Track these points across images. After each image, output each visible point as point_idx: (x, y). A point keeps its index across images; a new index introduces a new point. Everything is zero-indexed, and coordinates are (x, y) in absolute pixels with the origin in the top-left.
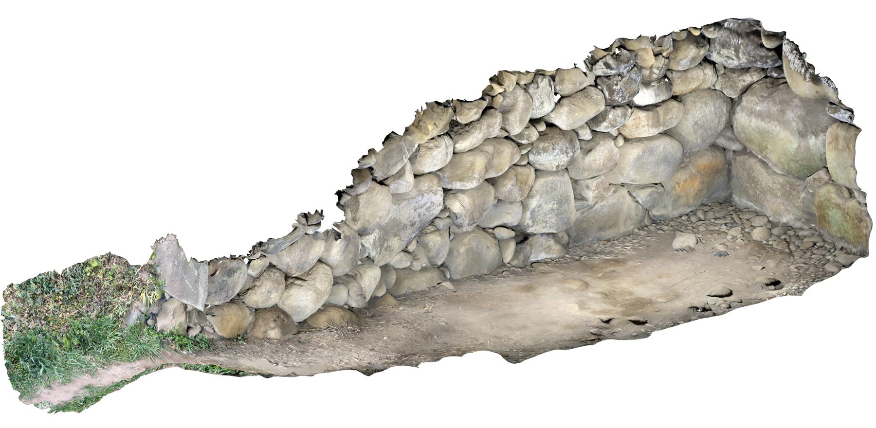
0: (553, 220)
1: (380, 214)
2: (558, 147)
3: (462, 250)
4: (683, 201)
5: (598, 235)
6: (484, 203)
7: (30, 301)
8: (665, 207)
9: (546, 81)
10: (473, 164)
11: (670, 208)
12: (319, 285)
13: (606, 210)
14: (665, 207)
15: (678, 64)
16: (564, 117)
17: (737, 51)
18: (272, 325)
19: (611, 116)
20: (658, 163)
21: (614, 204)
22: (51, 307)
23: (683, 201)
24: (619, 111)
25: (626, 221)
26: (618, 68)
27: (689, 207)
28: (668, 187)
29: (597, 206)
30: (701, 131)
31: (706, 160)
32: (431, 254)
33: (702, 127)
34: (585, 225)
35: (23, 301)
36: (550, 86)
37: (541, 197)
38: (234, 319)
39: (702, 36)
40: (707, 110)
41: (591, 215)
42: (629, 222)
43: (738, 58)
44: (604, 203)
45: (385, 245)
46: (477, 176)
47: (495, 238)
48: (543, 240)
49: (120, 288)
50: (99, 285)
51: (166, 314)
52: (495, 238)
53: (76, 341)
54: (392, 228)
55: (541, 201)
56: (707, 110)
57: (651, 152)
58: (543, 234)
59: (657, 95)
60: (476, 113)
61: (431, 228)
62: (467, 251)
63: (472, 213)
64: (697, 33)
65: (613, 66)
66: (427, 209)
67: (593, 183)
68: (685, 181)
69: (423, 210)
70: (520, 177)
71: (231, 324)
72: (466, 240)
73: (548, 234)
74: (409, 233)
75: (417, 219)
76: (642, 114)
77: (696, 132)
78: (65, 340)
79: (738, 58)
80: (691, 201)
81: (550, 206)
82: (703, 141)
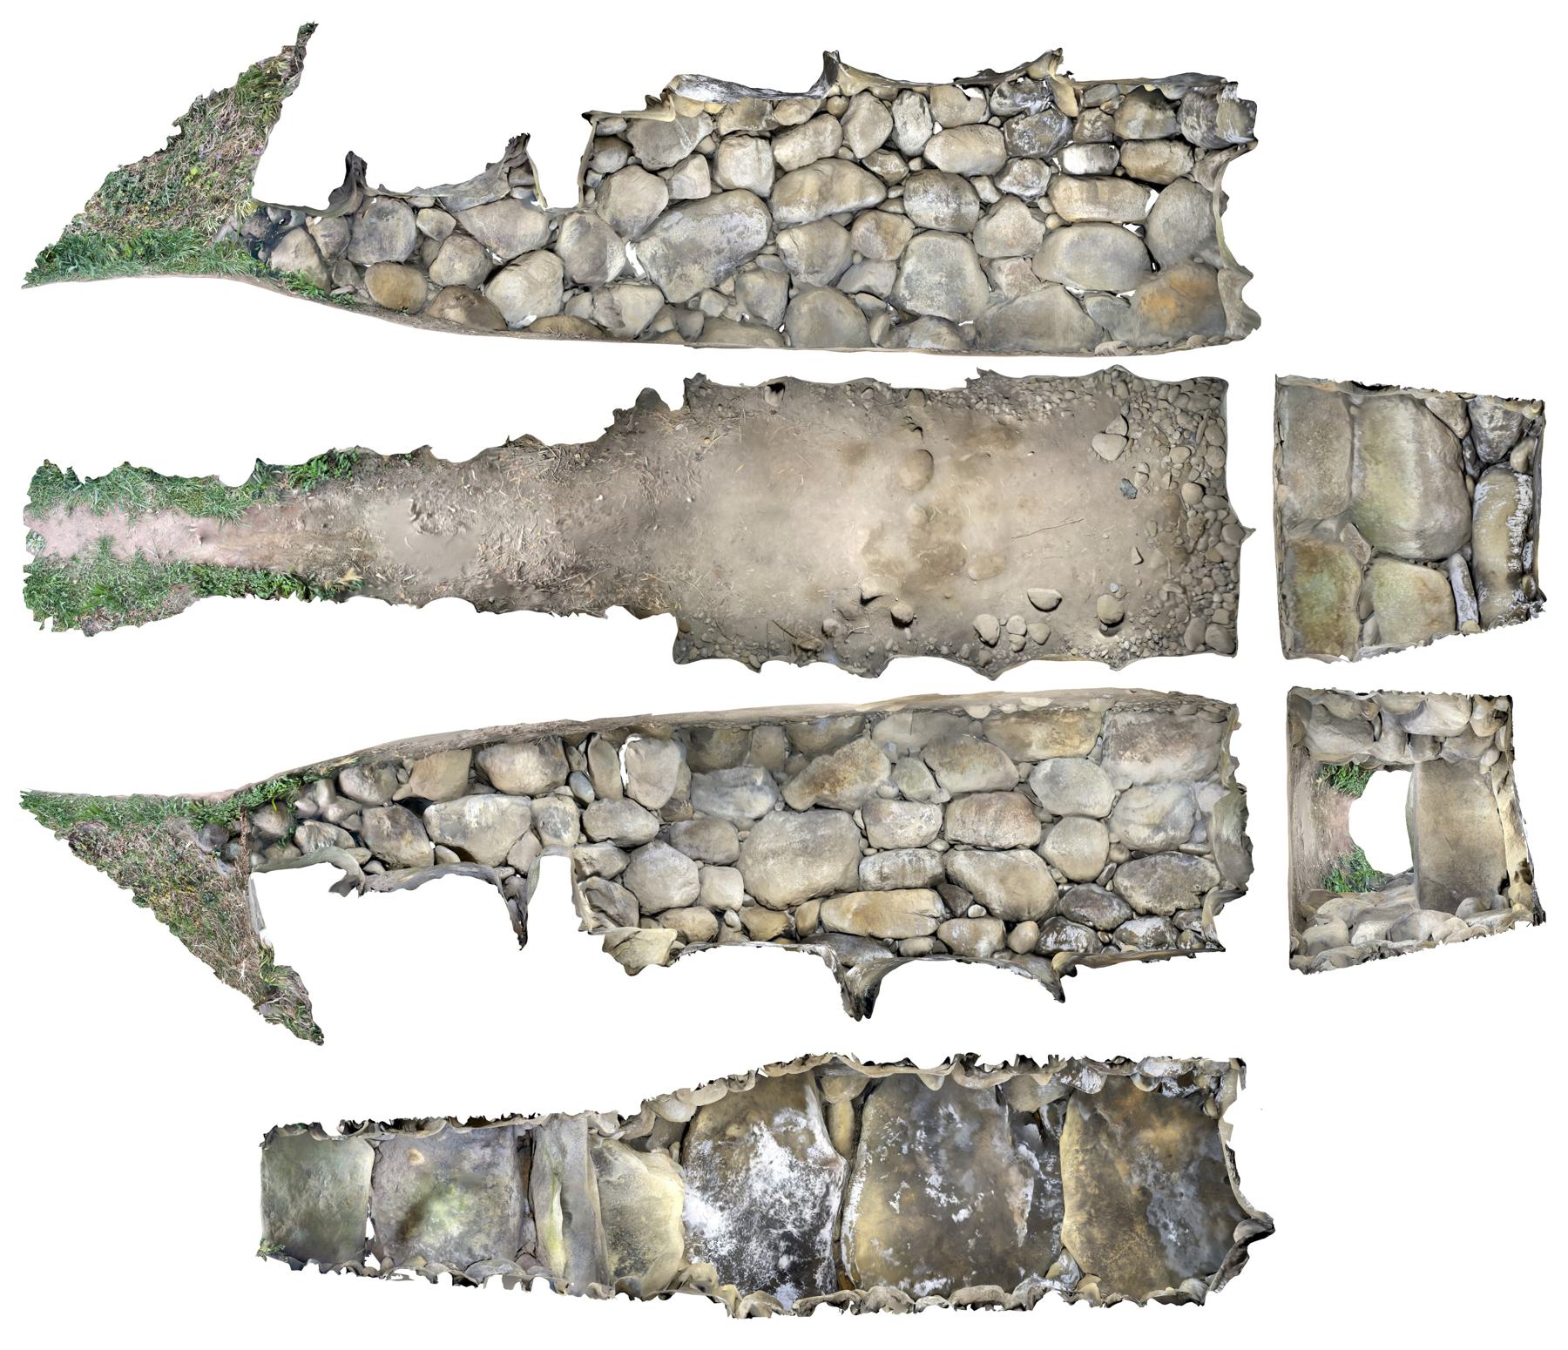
0: (942, 298)
1: (640, 205)
2: (932, 190)
3: (805, 309)
4: (1154, 325)
5: (1022, 341)
6: (828, 246)
7: (112, 211)
8: (1131, 330)
9: (915, 99)
10: (802, 184)
11: (1137, 334)
12: (533, 272)
13: (1031, 309)
14: (1131, 330)
15: (1126, 126)
16: (937, 150)
17: (1502, 428)
18: (452, 303)
19: (1015, 168)
20: (1105, 258)
21: (1042, 303)
22: (132, 217)
23: (1154, 325)
24: (1027, 164)
25: (1065, 332)
26: (1012, 97)
27: (1163, 335)
28: (1134, 306)
29: (1019, 301)
30: (1173, 233)
31: (1182, 275)
32: (750, 299)
33: (1174, 227)
34: (1003, 325)
35: (106, 211)
36: (922, 106)
37: (919, 261)
38: (392, 281)
39: (1158, 91)
40: (1181, 205)
41: (1010, 312)
42: (1071, 336)
43: (1494, 429)
44: (1028, 298)
45: (679, 270)
46: (805, 200)
47: (856, 304)
48: (931, 325)
49: (217, 201)
50: (194, 196)
51: (285, 249)
52: (856, 304)
53: (140, 251)
54: (690, 251)
55: (921, 267)
56: (1181, 205)
57: (1094, 241)
58: (931, 317)
59: (1090, 159)
60: (799, 112)
61: (751, 266)
62: (811, 310)
63: (810, 257)
64: (1149, 88)
65: (1007, 93)
66: (740, 234)
67: (1006, 265)
68: (1152, 295)
69: (733, 235)
70: (884, 225)
71: (387, 286)
72: (810, 297)
73: (940, 319)
74: (715, 265)
75: (725, 245)
76: (1074, 184)
77: (1167, 233)
78: (126, 247)
79: (1494, 429)
80: (1166, 328)
81: (937, 278)
82: (1177, 246)
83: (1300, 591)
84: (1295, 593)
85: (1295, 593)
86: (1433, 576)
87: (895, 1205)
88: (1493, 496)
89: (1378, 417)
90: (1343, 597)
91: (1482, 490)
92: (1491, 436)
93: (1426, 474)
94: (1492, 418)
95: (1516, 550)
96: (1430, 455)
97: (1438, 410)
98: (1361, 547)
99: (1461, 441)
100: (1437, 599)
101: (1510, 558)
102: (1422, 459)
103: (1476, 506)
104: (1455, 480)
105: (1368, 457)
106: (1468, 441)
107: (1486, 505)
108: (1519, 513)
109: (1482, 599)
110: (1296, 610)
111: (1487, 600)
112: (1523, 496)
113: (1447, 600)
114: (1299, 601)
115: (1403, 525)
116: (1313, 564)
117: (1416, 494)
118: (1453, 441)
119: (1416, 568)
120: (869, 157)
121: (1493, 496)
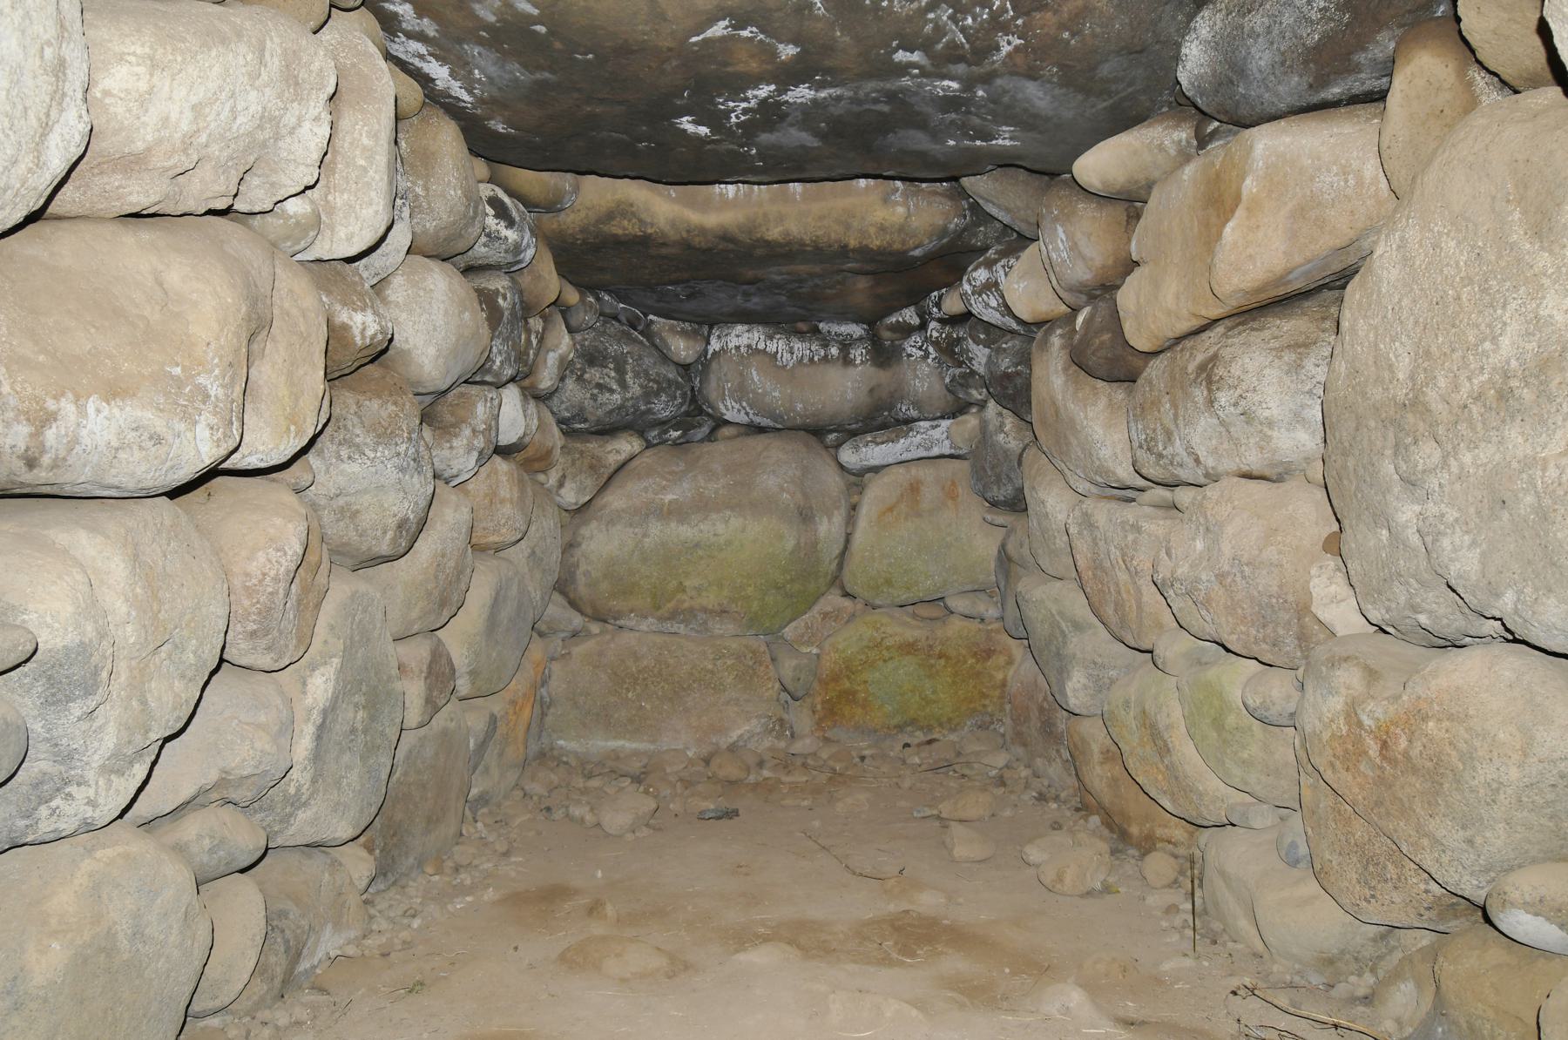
17: (620, 371)
43: (623, 385)
79: (623, 385)
83: (896, 720)
84: (899, 728)
85: (899, 728)
86: (876, 493)
87: (719, 29)
88: (741, 392)
89: (605, 586)
90: (909, 648)
91: (732, 411)
92: (635, 389)
93: (703, 506)
94: (601, 387)
95: (834, 351)
96: (669, 497)
97: (590, 484)
98: (825, 615)
99: (649, 445)
100: (914, 488)
101: (847, 361)
102: (676, 512)
103: (765, 422)
104: (720, 453)
105: (670, 605)
106: (653, 434)
107: (757, 405)
108: (772, 347)
109: (914, 413)
110: (930, 728)
111: (917, 404)
112: (744, 341)
113: (917, 472)
114: (913, 722)
115: (790, 544)
116: (849, 696)
117: (736, 522)
118: (648, 458)
119: (862, 523)
120: (1534, 83)
121: (741, 392)
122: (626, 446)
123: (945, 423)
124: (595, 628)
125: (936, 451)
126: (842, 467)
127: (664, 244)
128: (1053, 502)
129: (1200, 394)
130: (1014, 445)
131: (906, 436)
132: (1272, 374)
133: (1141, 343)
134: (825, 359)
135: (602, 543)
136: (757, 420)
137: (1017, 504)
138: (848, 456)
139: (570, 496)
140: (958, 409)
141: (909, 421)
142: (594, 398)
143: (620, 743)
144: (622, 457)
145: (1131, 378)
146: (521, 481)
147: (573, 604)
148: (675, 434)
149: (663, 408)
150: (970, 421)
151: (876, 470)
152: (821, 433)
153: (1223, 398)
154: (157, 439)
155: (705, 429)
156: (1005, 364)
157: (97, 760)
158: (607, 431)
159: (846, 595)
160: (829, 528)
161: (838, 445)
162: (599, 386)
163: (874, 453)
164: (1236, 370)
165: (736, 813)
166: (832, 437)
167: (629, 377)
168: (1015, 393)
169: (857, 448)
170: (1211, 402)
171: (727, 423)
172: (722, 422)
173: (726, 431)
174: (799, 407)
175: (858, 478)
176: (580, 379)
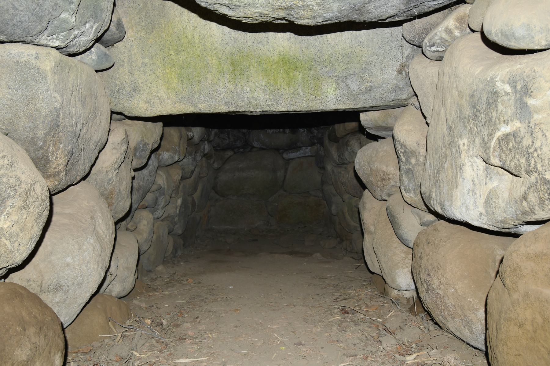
43: (229, 138)
79: (229, 138)
91: (256, 144)
96: (240, 166)
99: (235, 153)
103: (264, 147)
109: (301, 145)
122: (229, 153)
123: (309, 148)
124: (222, 199)
125: (307, 155)
126: (284, 158)
127: (283, 253)
128: (329, 167)
129: (346, 147)
130: (323, 154)
131: (299, 151)
132: (356, 144)
133: (338, 136)
134: (279, 132)
135: (224, 177)
136: (262, 147)
137: (324, 168)
138: (285, 156)
139: (216, 165)
140: (313, 144)
141: (300, 147)
142: (222, 141)
143: (228, 227)
144: (228, 156)
145: (338, 142)
146: (437, 183)
147: (216, 192)
148: (241, 150)
149: (239, 144)
150: (315, 147)
151: (292, 159)
152: (278, 150)
153: (349, 148)
154: (173, 157)
155: (249, 149)
156: (320, 135)
157: (161, 206)
158: (225, 149)
159: (285, 191)
160: (280, 174)
161: (283, 153)
162: (223, 139)
163: (292, 155)
164: (351, 143)
165: (257, 240)
166: (281, 151)
167: (230, 136)
168: (322, 143)
169: (287, 154)
170: (347, 149)
171: (255, 147)
172: (253, 147)
173: (254, 149)
174: (273, 144)
175: (288, 161)
176: (219, 137)
